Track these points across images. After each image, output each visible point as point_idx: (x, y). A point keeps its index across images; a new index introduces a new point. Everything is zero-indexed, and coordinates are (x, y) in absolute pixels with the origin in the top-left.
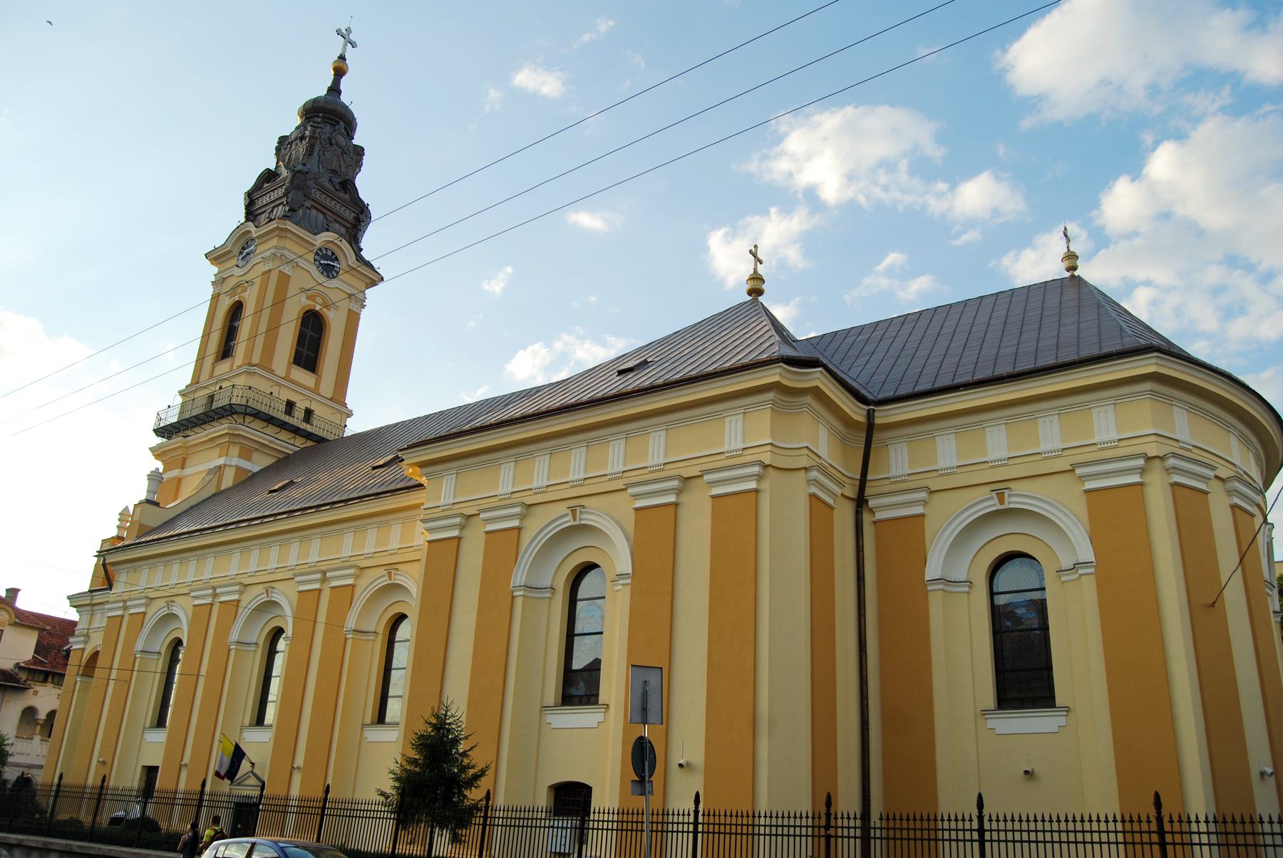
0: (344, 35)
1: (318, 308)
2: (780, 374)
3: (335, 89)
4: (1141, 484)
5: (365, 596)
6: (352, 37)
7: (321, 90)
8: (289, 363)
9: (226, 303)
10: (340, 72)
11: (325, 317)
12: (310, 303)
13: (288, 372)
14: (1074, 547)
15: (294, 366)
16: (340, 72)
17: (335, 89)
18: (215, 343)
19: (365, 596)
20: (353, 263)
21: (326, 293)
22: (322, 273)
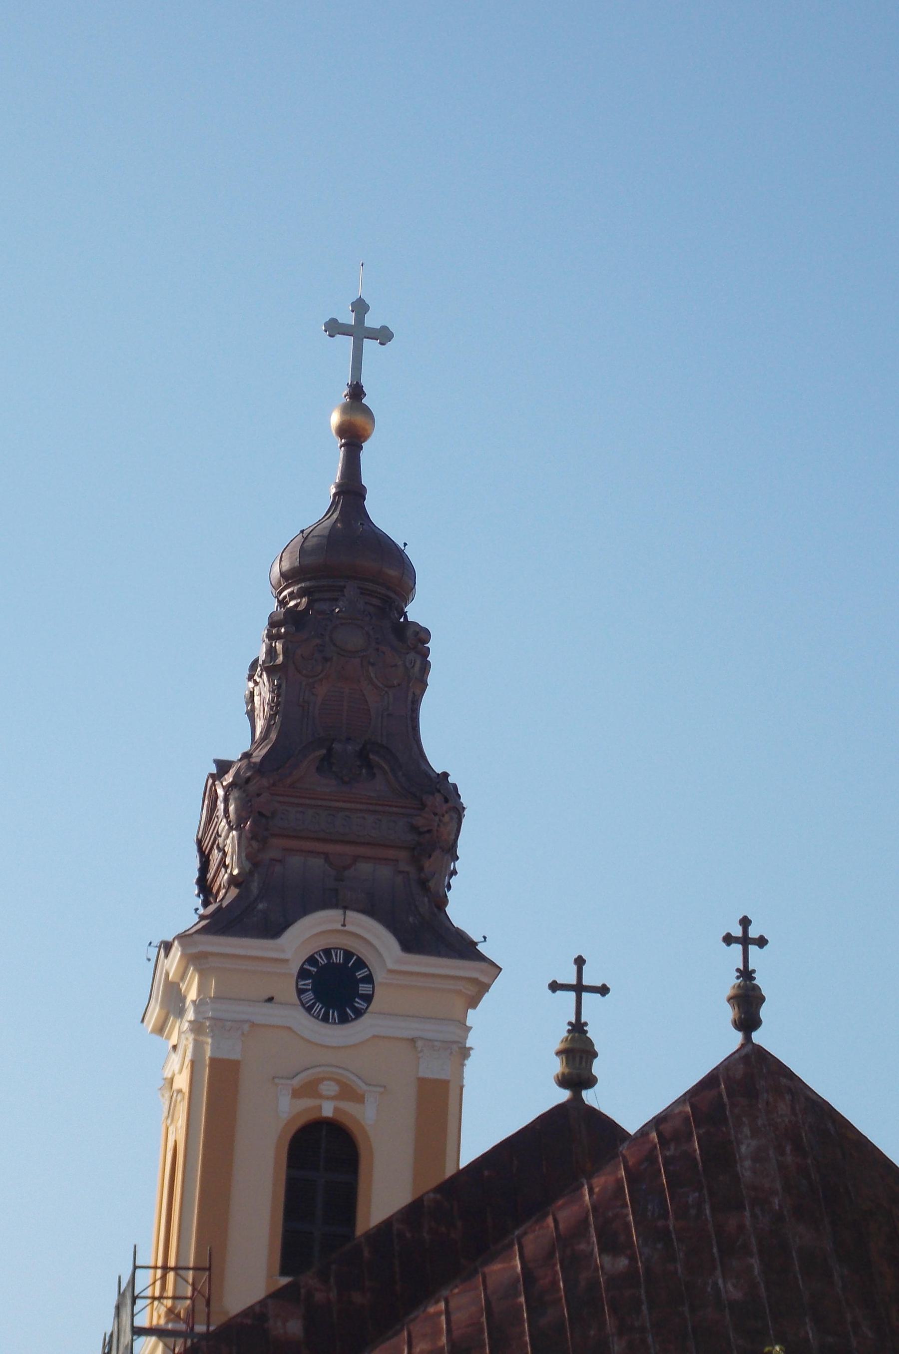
1: (328, 1110)
6: (372, 321)
22: (325, 1019)
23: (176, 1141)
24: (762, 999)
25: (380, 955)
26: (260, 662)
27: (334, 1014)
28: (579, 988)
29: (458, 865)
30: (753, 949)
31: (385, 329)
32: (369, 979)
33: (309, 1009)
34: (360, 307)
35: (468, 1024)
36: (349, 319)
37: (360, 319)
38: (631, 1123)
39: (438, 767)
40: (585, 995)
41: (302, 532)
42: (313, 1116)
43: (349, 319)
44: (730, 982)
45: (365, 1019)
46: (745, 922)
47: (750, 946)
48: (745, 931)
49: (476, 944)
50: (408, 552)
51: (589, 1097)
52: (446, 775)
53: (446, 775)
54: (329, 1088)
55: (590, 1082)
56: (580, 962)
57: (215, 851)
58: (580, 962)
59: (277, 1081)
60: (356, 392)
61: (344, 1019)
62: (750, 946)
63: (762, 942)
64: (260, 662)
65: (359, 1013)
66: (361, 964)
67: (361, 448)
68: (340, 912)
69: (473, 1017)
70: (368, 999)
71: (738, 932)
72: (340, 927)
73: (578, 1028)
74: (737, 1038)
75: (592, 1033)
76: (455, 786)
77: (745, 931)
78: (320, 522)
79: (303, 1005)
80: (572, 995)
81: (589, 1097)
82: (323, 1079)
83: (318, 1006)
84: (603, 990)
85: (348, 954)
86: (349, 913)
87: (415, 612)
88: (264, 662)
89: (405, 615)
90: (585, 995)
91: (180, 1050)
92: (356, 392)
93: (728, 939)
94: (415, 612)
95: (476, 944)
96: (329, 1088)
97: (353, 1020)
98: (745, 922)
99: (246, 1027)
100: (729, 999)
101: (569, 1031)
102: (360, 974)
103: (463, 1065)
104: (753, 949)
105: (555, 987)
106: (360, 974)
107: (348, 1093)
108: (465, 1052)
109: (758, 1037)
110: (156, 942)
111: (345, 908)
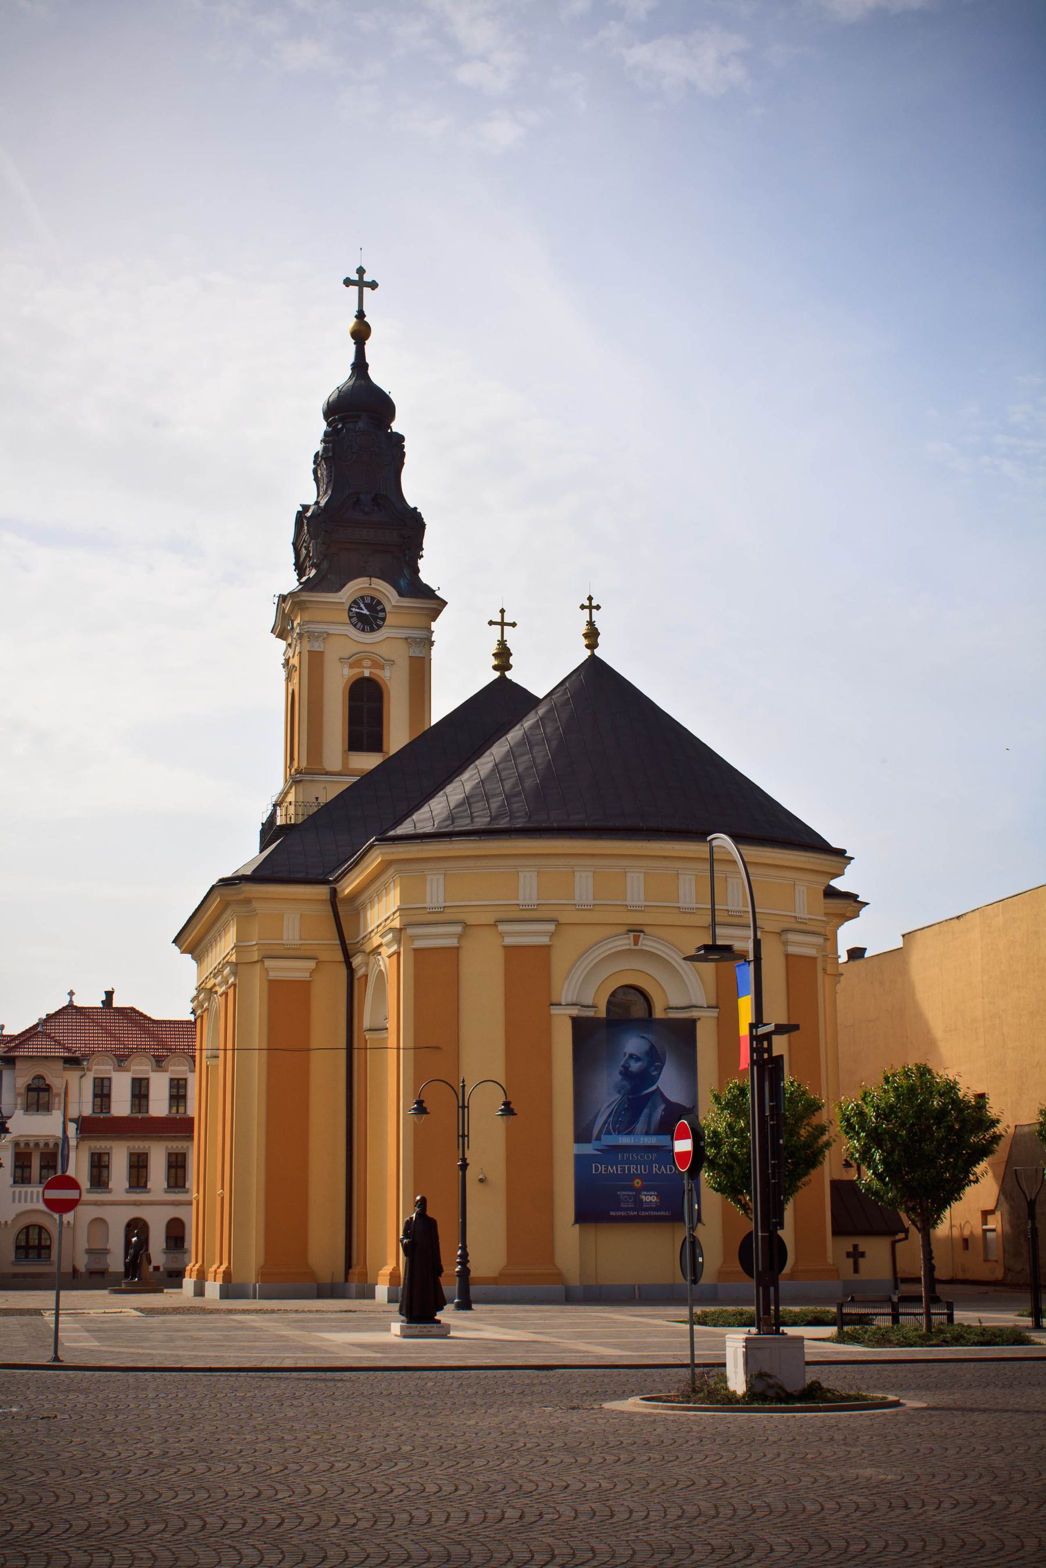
0: (361, 282)
1: (367, 674)
2: (381, 853)
3: (360, 366)
4: (549, 947)
5: (600, 954)
6: (367, 278)
7: (341, 375)
8: (344, 752)
9: (290, 691)
10: (361, 334)
11: (381, 682)
12: (356, 670)
13: (345, 762)
14: (668, 961)
15: (350, 753)
16: (361, 334)
17: (360, 366)
18: (340, 707)
19: (600, 954)
20: (397, 602)
21: (373, 651)
22: (363, 630)
23: (293, 690)
24: (599, 634)
25: (389, 600)
26: (320, 454)
27: (367, 628)
28: (502, 624)
29: (424, 553)
30: (594, 611)
31: (374, 281)
32: (383, 610)
33: (355, 626)
34: (361, 271)
35: (432, 630)
36: (355, 277)
37: (361, 277)
38: (540, 689)
39: (412, 504)
40: (500, 621)
41: (338, 388)
42: (360, 676)
43: (355, 277)
44: (584, 628)
45: (383, 630)
46: (590, 599)
47: (365, 288)
48: (590, 603)
49: (435, 591)
50: (391, 396)
51: (509, 674)
52: (416, 508)
53: (416, 508)
54: (367, 663)
55: (509, 667)
56: (502, 611)
57: (303, 549)
58: (502, 611)
59: (342, 660)
60: (361, 315)
61: (372, 630)
62: (365, 288)
63: (598, 607)
64: (320, 454)
65: (379, 627)
66: (379, 603)
67: (365, 343)
68: (368, 578)
69: (434, 626)
70: (384, 619)
71: (587, 603)
72: (368, 586)
73: (502, 643)
74: (588, 653)
75: (509, 645)
76: (420, 513)
77: (590, 603)
78: (346, 383)
79: (352, 624)
80: (499, 627)
81: (509, 674)
82: (363, 659)
83: (360, 624)
84: (514, 625)
85: (373, 598)
86: (372, 579)
87: (396, 427)
88: (322, 454)
89: (391, 428)
90: (500, 621)
91: (293, 646)
92: (361, 315)
93: (583, 607)
94: (396, 427)
95: (435, 591)
96: (367, 663)
97: (377, 630)
98: (590, 599)
99: (325, 635)
100: (848, 951)
101: (498, 645)
102: (379, 608)
103: (431, 649)
104: (594, 611)
105: (491, 623)
106: (379, 608)
107: (376, 665)
108: (432, 643)
109: (597, 652)
110: (277, 595)
111: (370, 577)
